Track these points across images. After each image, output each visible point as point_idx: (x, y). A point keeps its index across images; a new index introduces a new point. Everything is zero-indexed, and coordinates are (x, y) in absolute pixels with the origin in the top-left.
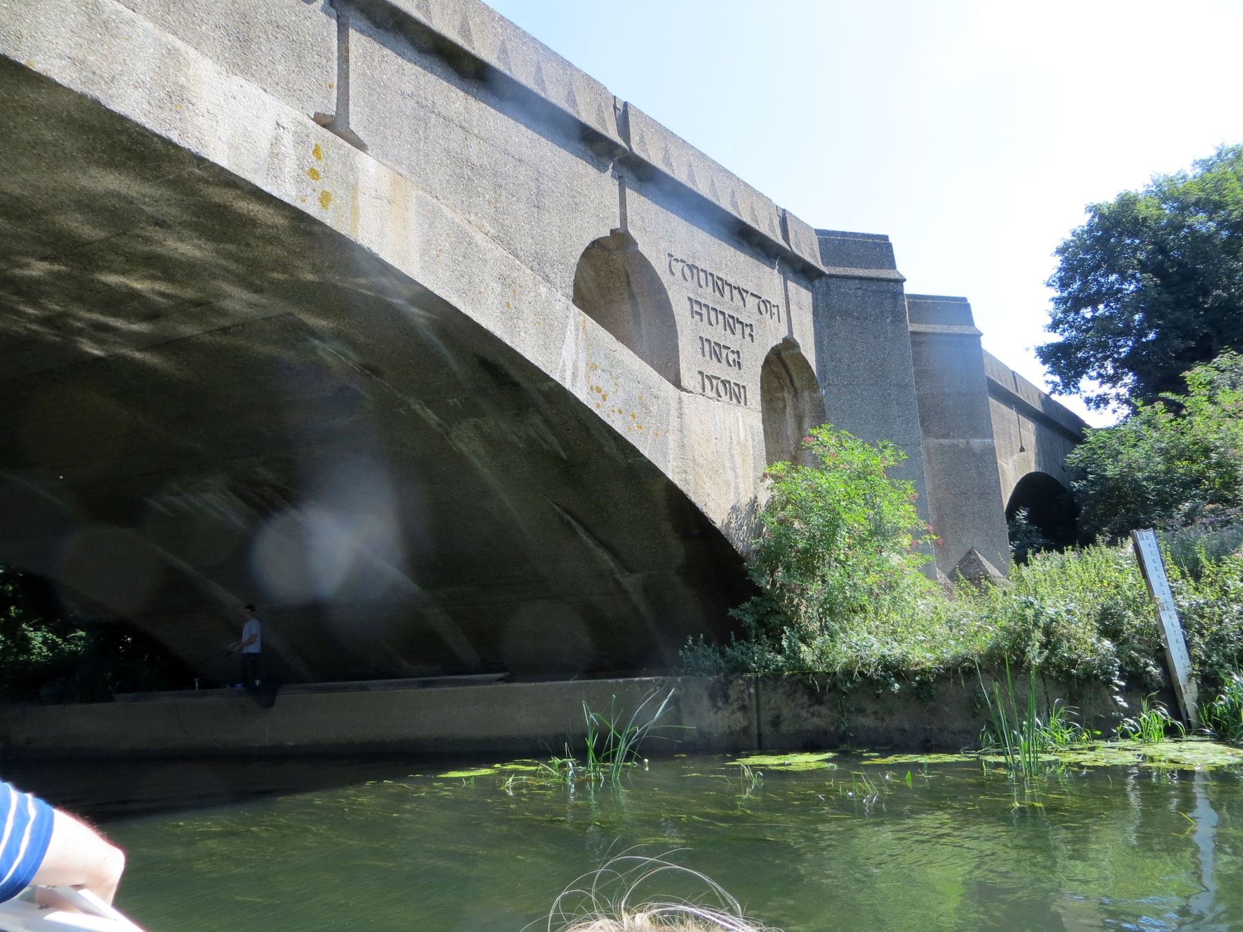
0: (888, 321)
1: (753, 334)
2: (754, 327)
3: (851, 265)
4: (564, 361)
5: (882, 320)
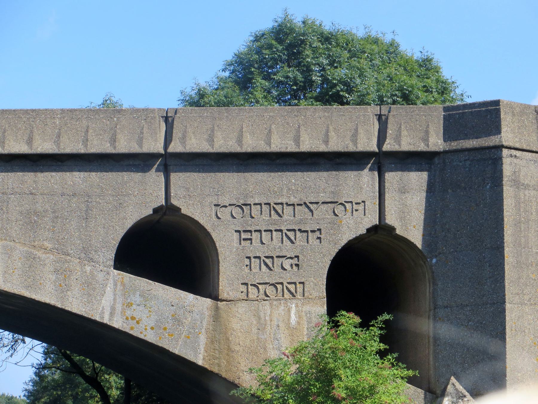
0: (488, 187)
1: (322, 236)
2: (322, 231)
3: (466, 137)
4: (103, 307)
5: (483, 188)
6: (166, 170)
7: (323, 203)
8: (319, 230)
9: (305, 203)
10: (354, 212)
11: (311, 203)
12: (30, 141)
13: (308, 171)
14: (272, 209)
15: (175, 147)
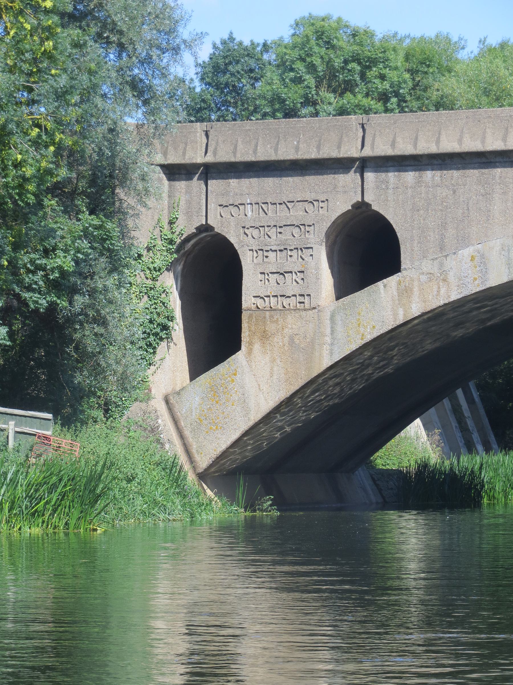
6: (362, 171)
7: (298, 201)
8: (313, 224)
9: (284, 202)
10: (320, 209)
11: (288, 202)
12: (460, 141)
13: (264, 177)
14: (260, 207)
15: (367, 152)
